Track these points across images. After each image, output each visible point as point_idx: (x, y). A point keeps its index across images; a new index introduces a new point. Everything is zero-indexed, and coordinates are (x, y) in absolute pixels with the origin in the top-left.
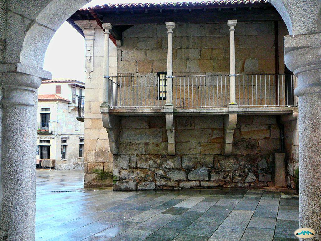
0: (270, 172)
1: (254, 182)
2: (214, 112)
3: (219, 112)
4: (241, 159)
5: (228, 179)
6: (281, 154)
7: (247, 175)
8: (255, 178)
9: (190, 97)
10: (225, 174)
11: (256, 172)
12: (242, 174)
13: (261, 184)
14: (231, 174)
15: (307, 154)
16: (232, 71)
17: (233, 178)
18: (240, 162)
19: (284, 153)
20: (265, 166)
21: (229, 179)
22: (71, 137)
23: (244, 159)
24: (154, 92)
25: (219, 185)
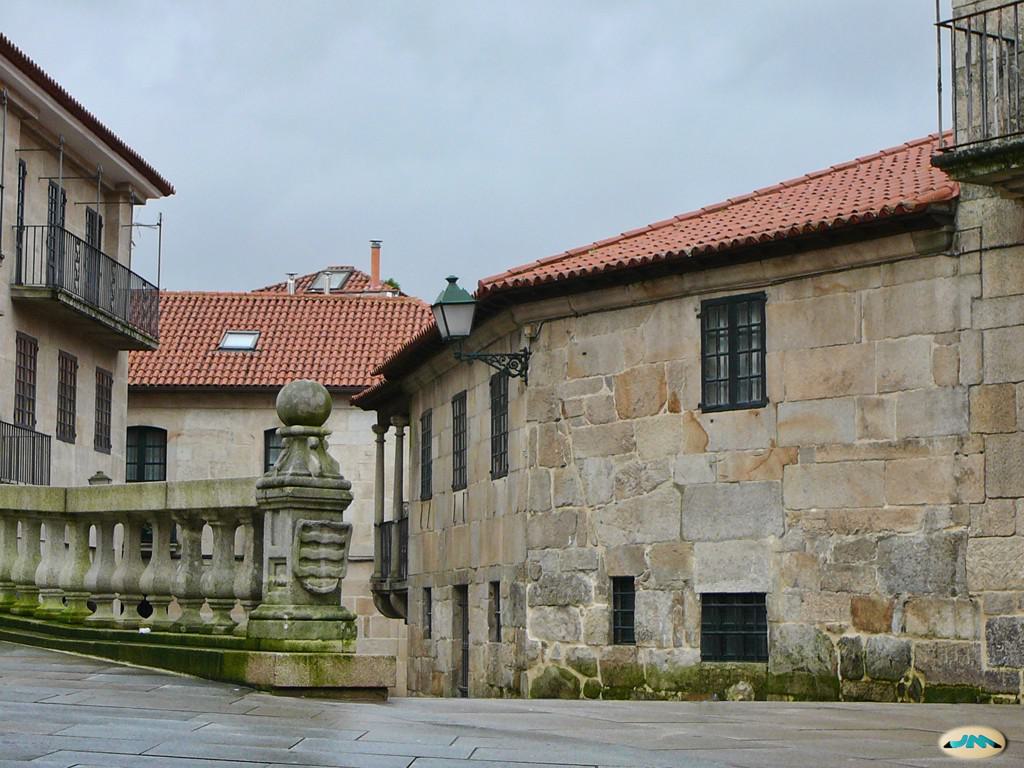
9: (918, 646)
24: (892, 640)
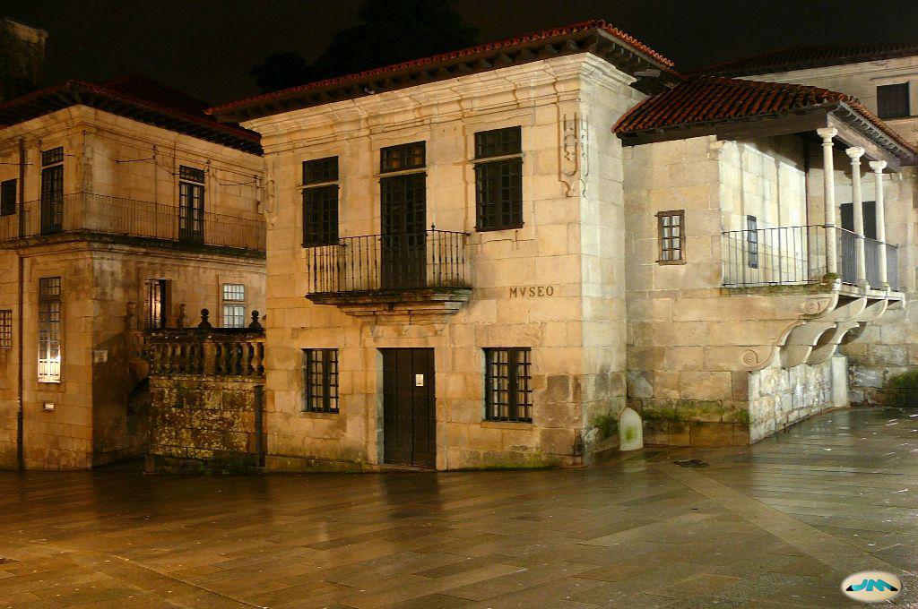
22: (179, 163)
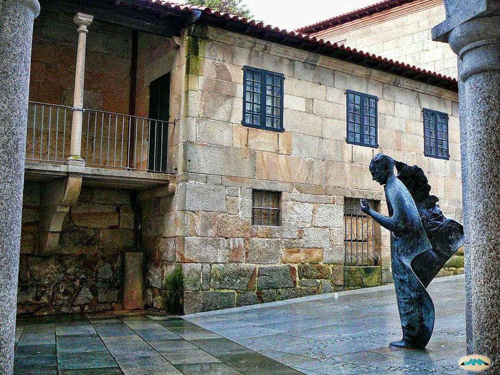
0: (116, 284)
1: (90, 304)
2: (42, 171)
3: (51, 171)
4: (69, 263)
5: (45, 299)
6: (137, 254)
7: (78, 291)
8: (91, 296)
10: (39, 291)
11: (93, 286)
12: (70, 290)
13: (101, 307)
14: (50, 290)
15: (494, 139)
16: (78, 101)
17: (53, 299)
18: (68, 269)
19: (140, 252)
20: (109, 275)
21: (46, 300)
23: (73, 263)
25: (26, 312)
